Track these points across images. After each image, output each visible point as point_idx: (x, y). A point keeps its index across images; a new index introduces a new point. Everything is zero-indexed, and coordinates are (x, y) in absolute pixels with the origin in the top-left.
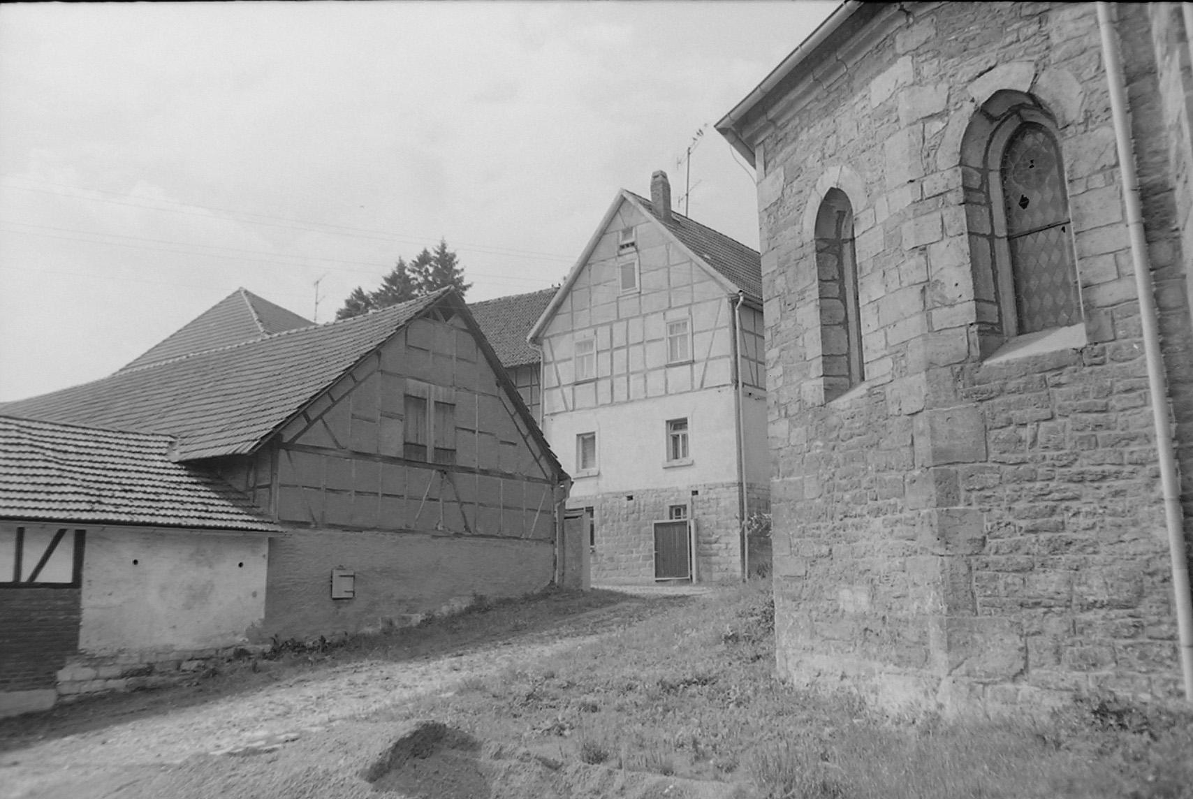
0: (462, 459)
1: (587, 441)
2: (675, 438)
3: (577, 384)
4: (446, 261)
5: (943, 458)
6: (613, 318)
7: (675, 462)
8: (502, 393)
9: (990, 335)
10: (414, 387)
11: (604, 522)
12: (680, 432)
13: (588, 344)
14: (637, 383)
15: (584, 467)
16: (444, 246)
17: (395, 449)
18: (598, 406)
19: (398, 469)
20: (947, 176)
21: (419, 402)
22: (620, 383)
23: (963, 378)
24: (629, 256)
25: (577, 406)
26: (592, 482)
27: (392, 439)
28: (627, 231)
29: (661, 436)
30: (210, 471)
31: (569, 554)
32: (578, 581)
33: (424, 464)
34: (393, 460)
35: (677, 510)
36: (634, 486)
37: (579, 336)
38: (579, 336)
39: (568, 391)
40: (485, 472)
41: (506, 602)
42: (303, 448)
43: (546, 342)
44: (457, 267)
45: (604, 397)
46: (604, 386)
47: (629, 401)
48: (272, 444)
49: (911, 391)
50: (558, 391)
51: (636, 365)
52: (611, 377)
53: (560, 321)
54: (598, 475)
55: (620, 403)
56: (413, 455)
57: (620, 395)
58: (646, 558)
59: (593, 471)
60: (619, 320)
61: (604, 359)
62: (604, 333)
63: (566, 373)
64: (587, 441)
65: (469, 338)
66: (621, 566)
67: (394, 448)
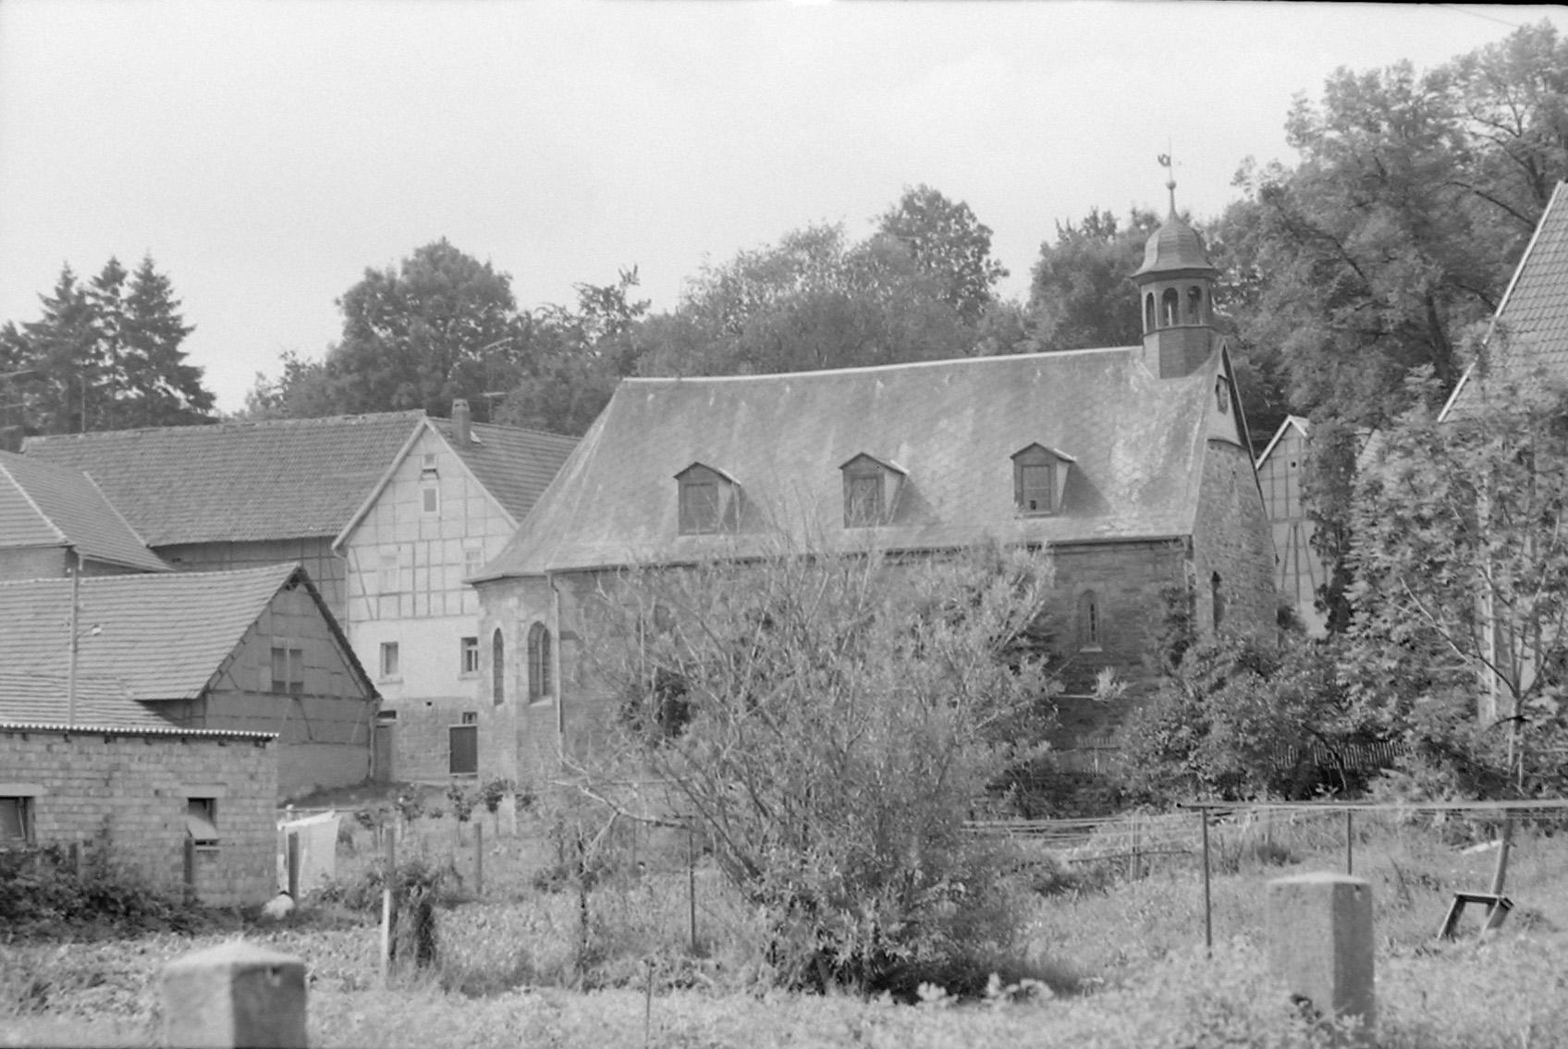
0: (308, 688)
1: (390, 649)
2: (469, 653)
3: (382, 595)
4: (152, 289)
5: (519, 733)
6: (415, 537)
7: (469, 674)
8: (333, 637)
9: (534, 696)
10: (277, 641)
11: (405, 724)
12: (473, 648)
13: (390, 559)
14: (436, 601)
15: (388, 672)
16: (149, 264)
17: (267, 687)
18: (400, 618)
19: (268, 699)
20: (524, 643)
21: (278, 652)
22: (422, 598)
23: (524, 708)
24: (431, 482)
25: (382, 615)
26: (395, 687)
27: (265, 680)
28: (430, 458)
29: (456, 653)
30: (158, 707)
31: (381, 755)
32: (387, 775)
33: (285, 695)
34: (267, 694)
35: (470, 716)
36: (433, 693)
37: (385, 550)
38: (385, 550)
39: (372, 601)
40: (322, 697)
41: (337, 790)
42: (219, 692)
43: (350, 551)
44: (171, 299)
45: (407, 611)
46: (407, 600)
47: (429, 616)
48: (206, 691)
49: (513, 710)
50: (363, 600)
51: (436, 585)
52: (414, 594)
53: (365, 533)
54: (401, 682)
55: (421, 618)
56: (278, 687)
57: (422, 610)
58: (443, 757)
59: (394, 677)
60: (421, 540)
61: (407, 575)
62: (406, 549)
63: (371, 583)
64: (390, 649)
65: (310, 599)
66: (421, 761)
67: (267, 686)
